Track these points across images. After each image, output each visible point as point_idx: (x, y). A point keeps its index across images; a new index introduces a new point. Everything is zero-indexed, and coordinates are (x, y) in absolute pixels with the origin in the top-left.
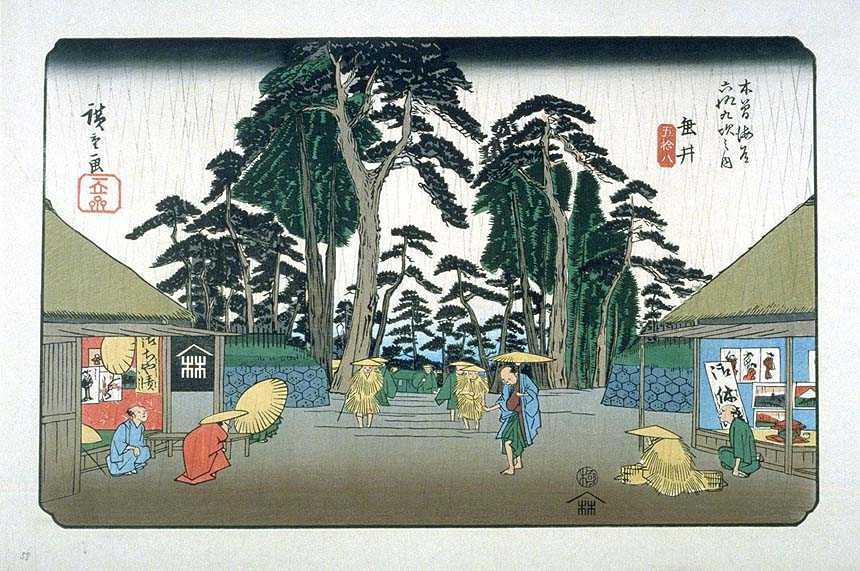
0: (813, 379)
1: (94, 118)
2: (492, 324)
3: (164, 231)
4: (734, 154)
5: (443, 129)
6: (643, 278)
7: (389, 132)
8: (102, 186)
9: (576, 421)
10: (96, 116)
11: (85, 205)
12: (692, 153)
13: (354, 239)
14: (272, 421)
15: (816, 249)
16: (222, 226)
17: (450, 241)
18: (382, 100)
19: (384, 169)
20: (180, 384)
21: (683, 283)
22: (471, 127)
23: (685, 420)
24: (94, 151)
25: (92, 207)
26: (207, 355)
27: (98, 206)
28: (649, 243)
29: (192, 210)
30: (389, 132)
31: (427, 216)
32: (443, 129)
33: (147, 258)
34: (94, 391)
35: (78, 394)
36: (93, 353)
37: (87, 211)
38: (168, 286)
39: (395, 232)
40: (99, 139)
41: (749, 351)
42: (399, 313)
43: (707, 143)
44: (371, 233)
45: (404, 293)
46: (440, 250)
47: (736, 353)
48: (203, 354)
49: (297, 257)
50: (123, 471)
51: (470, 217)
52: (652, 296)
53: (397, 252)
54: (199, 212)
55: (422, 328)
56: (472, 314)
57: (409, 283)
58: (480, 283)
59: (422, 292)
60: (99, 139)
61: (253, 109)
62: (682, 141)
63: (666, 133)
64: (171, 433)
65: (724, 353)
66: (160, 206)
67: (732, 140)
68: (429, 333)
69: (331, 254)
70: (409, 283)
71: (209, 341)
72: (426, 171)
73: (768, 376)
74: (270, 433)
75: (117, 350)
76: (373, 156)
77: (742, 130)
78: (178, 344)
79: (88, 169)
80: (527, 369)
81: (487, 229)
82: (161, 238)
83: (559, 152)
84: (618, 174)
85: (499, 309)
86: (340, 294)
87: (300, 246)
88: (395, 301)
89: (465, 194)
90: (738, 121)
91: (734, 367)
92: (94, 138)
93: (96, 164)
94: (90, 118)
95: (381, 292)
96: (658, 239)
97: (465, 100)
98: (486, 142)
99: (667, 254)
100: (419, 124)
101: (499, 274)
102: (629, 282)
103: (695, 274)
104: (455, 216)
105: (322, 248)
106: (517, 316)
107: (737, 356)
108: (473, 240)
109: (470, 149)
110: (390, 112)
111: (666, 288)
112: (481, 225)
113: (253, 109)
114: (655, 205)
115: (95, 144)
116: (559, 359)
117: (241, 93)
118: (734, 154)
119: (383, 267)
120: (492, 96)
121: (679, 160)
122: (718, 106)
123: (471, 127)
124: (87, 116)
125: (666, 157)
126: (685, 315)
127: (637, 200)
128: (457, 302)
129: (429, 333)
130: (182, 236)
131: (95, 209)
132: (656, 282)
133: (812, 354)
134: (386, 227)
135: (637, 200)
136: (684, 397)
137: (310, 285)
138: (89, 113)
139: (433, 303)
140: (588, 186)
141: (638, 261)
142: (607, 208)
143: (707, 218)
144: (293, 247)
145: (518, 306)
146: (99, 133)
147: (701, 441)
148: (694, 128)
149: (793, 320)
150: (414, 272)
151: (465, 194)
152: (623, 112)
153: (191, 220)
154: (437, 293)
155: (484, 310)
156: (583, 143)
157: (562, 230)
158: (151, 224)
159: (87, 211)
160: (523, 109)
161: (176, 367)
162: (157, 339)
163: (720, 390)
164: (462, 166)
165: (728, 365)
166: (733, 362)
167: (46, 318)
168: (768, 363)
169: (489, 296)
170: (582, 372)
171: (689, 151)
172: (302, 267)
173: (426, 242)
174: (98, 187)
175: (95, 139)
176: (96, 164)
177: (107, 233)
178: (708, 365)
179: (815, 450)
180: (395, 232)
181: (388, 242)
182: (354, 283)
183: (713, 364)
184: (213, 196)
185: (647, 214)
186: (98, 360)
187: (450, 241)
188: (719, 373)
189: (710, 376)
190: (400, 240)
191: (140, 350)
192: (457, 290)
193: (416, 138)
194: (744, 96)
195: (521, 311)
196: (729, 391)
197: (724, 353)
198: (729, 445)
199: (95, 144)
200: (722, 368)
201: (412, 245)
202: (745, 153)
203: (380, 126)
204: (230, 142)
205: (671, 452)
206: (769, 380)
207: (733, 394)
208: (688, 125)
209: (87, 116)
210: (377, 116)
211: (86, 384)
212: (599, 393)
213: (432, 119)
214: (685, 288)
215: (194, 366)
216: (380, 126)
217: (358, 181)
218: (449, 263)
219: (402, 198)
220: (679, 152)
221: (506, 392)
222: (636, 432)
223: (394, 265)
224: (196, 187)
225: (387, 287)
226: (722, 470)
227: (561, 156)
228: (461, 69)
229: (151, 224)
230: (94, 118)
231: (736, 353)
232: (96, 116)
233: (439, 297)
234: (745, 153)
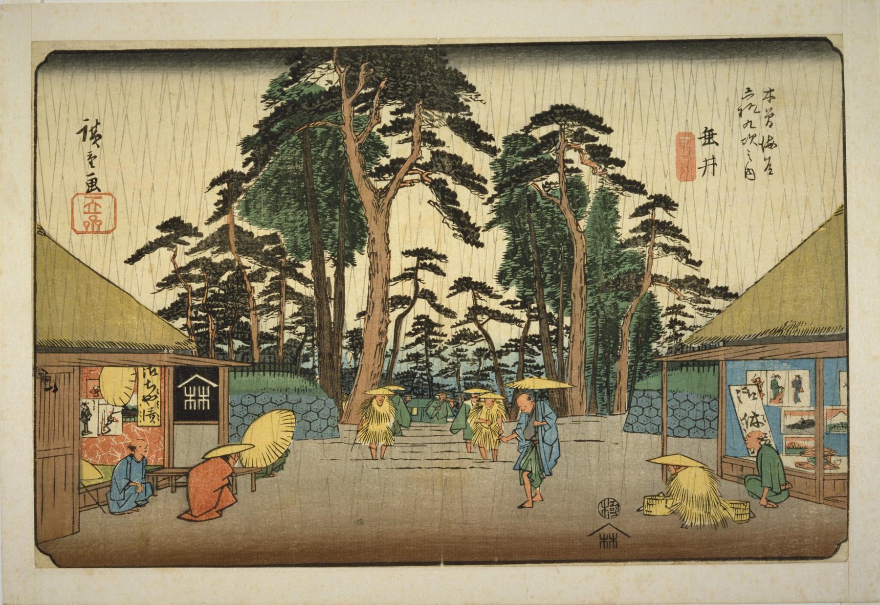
0: (844, 401)
1: (89, 135)
2: (508, 348)
3: (164, 253)
4: (758, 165)
5: (456, 145)
6: (664, 297)
7: (397, 147)
8: (96, 204)
9: (607, 455)
10: (91, 134)
11: (79, 227)
12: (714, 164)
13: (362, 260)
14: (280, 455)
15: (846, 243)
16: (224, 248)
17: (463, 261)
18: (392, 113)
19: (393, 188)
20: (183, 414)
21: (709, 302)
22: (474, 135)
23: (709, 448)
24: (91, 171)
25: (87, 227)
26: (211, 387)
27: (94, 228)
28: (671, 258)
29: (195, 233)
30: (397, 147)
31: (436, 233)
32: (456, 145)
33: (145, 286)
34: (93, 425)
35: (76, 428)
36: (92, 385)
37: (82, 233)
38: (169, 314)
39: (407, 253)
40: (95, 157)
41: (776, 373)
42: (413, 340)
43: (731, 149)
44: (378, 247)
45: (418, 318)
46: (453, 273)
47: (762, 375)
48: (206, 385)
49: (300, 278)
50: (123, 509)
51: (483, 237)
52: (674, 317)
53: (409, 275)
54: (201, 235)
55: (438, 354)
56: (488, 338)
57: (422, 307)
58: (494, 305)
59: (434, 316)
60: (95, 157)
61: (255, 126)
62: (702, 152)
63: (685, 143)
64: (173, 468)
65: (751, 376)
66: (163, 227)
67: (756, 151)
68: (444, 359)
69: (340, 277)
70: (422, 307)
71: (213, 373)
72: (438, 187)
73: (797, 399)
74: (278, 467)
75: (116, 383)
76: (380, 172)
77: (766, 140)
78: (181, 373)
79: (84, 188)
80: (542, 395)
81: (503, 246)
82: (162, 262)
83: (575, 166)
84: (637, 187)
85: (516, 332)
86: (351, 323)
87: (307, 269)
88: (408, 324)
89: (476, 207)
90: (763, 132)
91: (760, 391)
92: (90, 157)
93: (92, 184)
94: (85, 133)
95: (394, 316)
96: (683, 253)
97: (479, 114)
98: (499, 156)
99: (686, 271)
100: (429, 138)
101: (512, 293)
102: (651, 304)
103: (723, 292)
104: (469, 233)
105: (330, 271)
106: (533, 340)
107: (763, 378)
108: (488, 258)
109: (481, 164)
110: (397, 127)
111: (689, 309)
112: (497, 241)
113: (255, 126)
114: (677, 219)
115: (91, 163)
116: (575, 385)
117: (243, 103)
118: (758, 165)
119: (395, 290)
120: (505, 102)
121: (700, 172)
122: (740, 115)
123: (474, 135)
124: (82, 134)
125: (686, 171)
126: (708, 334)
127: (660, 214)
128: (472, 327)
129: (444, 359)
130: (183, 261)
131: (90, 229)
132: (678, 303)
133: (843, 375)
134: (396, 248)
135: (660, 214)
136: (711, 417)
137: (322, 313)
138: (84, 130)
139: (448, 328)
140: (607, 202)
141: (656, 279)
142: (627, 226)
143: (732, 235)
144: (299, 270)
145: (535, 328)
146: (95, 151)
147: (727, 468)
148: (715, 138)
149: (823, 347)
150: (430, 296)
151: (476, 207)
152: (646, 124)
153: (193, 241)
154: (451, 317)
155: (501, 334)
156: (601, 155)
157: (553, 206)
158: (150, 248)
159: (82, 233)
160: (539, 120)
161: (179, 396)
162: (158, 369)
163: (746, 415)
164: (467, 176)
165: (753, 389)
166: (758, 383)
167: (38, 348)
168: (797, 384)
169: (509, 319)
170: (602, 398)
171: (712, 163)
172: (308, 292)
173: (434, 261)
174: (92, 206)
175: (91, 157)
176: (92, 184)
177: (105, 256)
178: (733, 389)
179: (846, 477)
180: (407, 253)
181: (399, 264)
182: (365, 309)
183: (738, 388)
184: (216, 216)
185: (666, 228)
186: (97, 393)
187: (463, 261)
188: (744, 397)
189: (736, 400)
190: (412, 262)
191: (142, 381)
192: (475, 311)
193: (426, 156)
194: (767, 105)
195: (538, 333)
196: (756, 415)
197: (751, 376)
198: (756, 473)
199: (91, 163)
200: (748, 392)
201: (424, 267)
202: (769, 165)
203: (387, 140)
204: (236, 161)
205: (694, 481)
206: (798, 404)
207: (760, 419)
208: (709, 135)
209: (82, 134)
210: (385, 130)
211: (86, 416)
212: (618, 420)
213: (444, 133)
214: (711, 307)
215: (197, 398)
216: (387, 140)
217: (367, 197)
218: (463, 284)
219: (412, 217)
220: (700, 163)
221: (523, 419)
222: (657, 461)
223: (406, 288)
224: (199, 208)
225: (400, 311)
226: (750, 499)
227: (577, 170)
228: (464, 71)
229: (150, 248)
230: (89, 135)
231: (762, 375)
232: (91, 134)
233: (454, 321)
234: (769, 165)
